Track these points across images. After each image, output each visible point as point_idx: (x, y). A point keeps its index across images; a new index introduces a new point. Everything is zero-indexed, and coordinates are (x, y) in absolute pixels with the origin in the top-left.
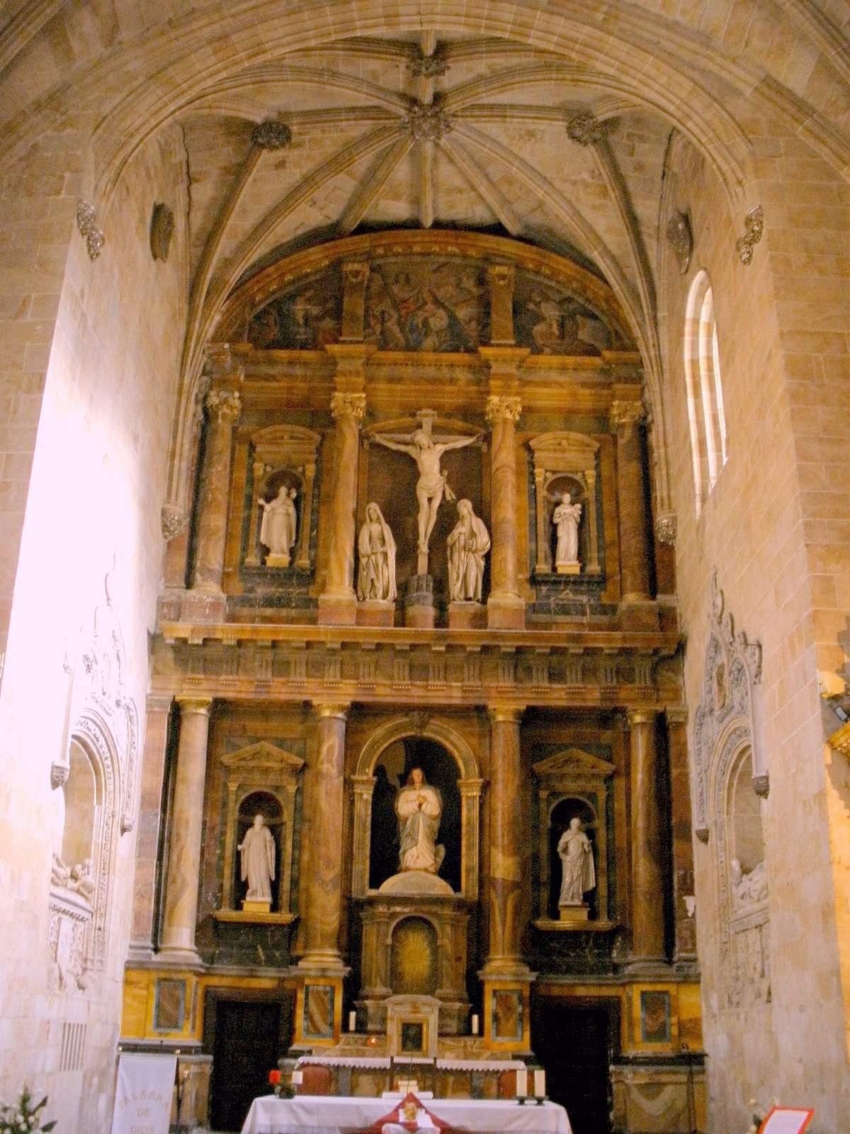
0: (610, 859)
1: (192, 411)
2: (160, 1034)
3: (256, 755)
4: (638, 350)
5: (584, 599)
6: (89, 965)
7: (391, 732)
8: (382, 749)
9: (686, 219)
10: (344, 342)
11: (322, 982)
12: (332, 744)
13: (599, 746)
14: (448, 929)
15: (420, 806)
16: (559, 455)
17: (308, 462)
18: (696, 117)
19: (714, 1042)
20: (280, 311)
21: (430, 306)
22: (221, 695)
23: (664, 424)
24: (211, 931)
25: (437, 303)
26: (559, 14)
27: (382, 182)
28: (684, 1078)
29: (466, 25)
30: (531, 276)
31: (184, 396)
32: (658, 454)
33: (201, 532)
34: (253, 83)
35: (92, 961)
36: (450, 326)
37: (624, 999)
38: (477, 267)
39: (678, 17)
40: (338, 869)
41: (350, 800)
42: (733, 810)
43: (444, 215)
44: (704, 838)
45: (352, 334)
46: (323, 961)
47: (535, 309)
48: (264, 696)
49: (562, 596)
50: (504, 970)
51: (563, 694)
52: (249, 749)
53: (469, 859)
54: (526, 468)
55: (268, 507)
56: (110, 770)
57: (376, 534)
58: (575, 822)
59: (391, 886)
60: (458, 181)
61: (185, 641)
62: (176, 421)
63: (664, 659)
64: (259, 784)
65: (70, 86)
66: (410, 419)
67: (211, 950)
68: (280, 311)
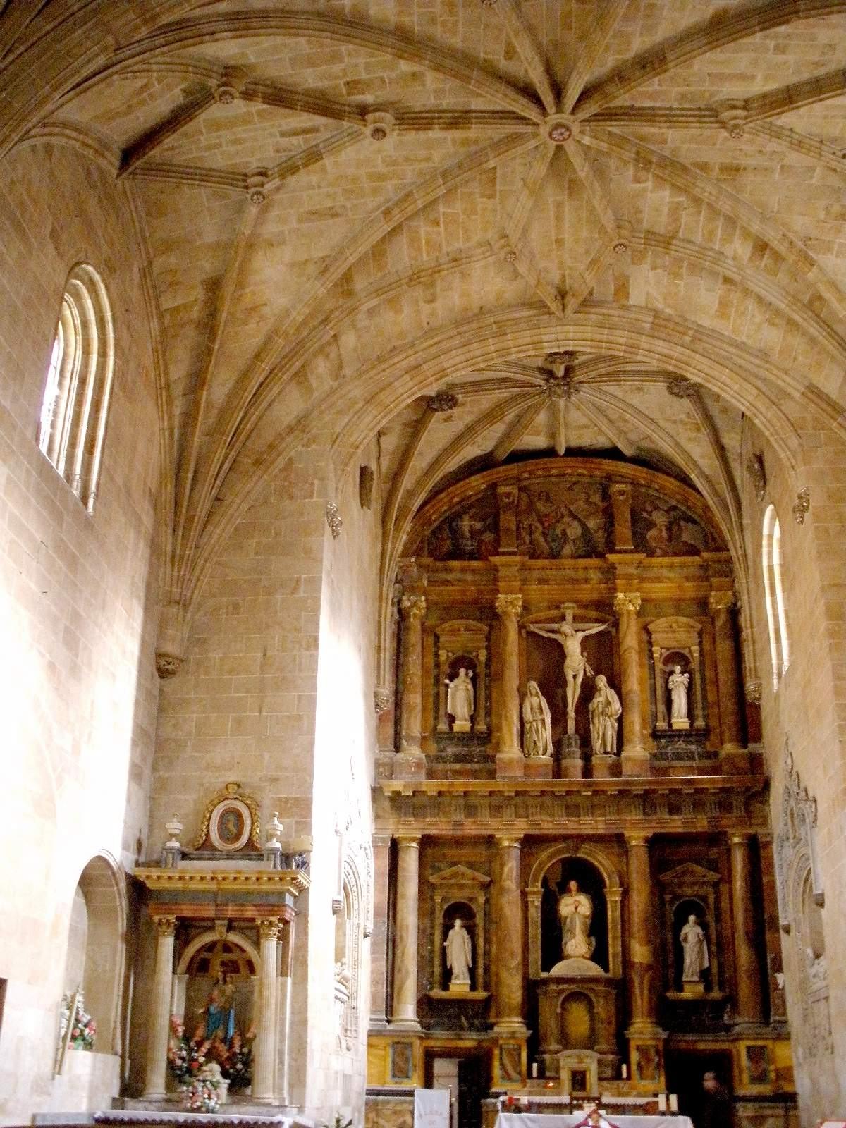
0: (719, 945)
1: (390, 611)
2: (396, 1083)
3: (454, 875)
4: (728, 550)
5: (693, 747)
6: (349, 1033)
8: (547, 867)
9: (760, 459)
11: (512, 1041)
12: (511, 866)
13: (708, 860)
14: (602, 1001)
15: (576, 908)
17: (480, 648)
18: (761, 416)
19: (802, 1084)
20: (452, 530)
21: (567, 519)
22: (427, 832)
23: (751, 610)
24: (426, 1005)
25: (573, 516)
26: (658, 338)
27: (526, 427)
28: (781, 1112)
29: (591, 347)
30: (643, 490)
31: (384, 601)
32: (746, 633)
33: (404, 708)
36: (583, 535)
37: (734, 1051)
38: (601, 484)
39: (744, 339)
40: (519, 958)
41: (525, 906)
42: (807, 911)
43: (575, 443)
44: (788, 931)
45: (509, 545)
46: (511, 1026)
48: (459, 833)
49: (676, 746)
50: (643, 1030)
51: (679, 823)
52: (448, 872)
53: (614, 948)
54: (646, 647)
55: (452, 685)
58: (692, 918)
59: (558, 970)
60: (584, 421)
61: (398, 793)
62: (379, 622)
63: (754, 795)
64: (458, 896)
66: (556, 611)
67: (428, 1020)
68: (451, 526)
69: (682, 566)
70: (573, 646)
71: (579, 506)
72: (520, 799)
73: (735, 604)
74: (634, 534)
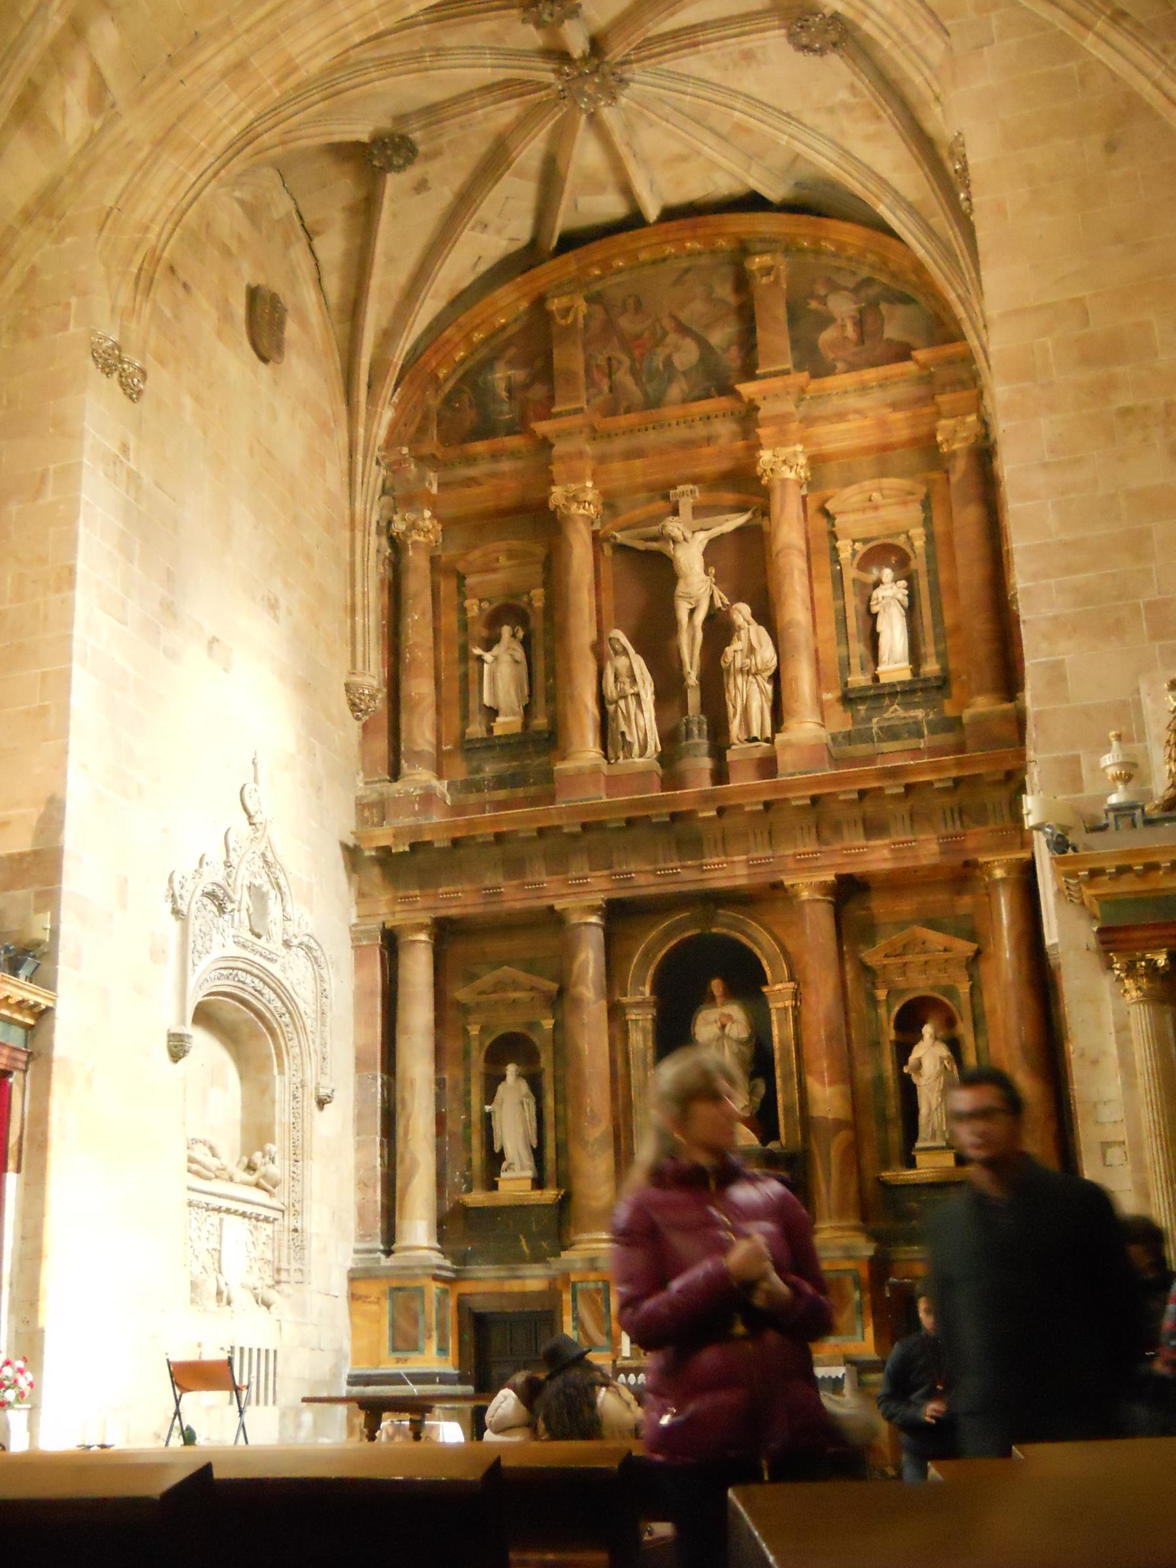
1: (374, 545)
2: (398, 1360)
5: (919, 713)
6: (284, 1276)
7: (668, 934)
10: (560, 415)
11: (593, 1276)
12: (589, 958)
15: (723, 1027)
16: (870, 514)
21: (672, 337)
24: (453, 1223)
25: (683, 330)
34: (324, 99)
35: (288, 1270)
36: (702, 360)
43: (677, 197)
47: (820, 307)
51: (886, 853)
55: (488, 657)
56: (291, 1028)
57: (623, 670)
61: (387, 850)
64: (509, 1023)
65: (61, 180)
69: (882, 385)
70: (690, 558)
71: (694, 310)
72: (595, 837)
73: (987, 436)
74: (795, 343)
